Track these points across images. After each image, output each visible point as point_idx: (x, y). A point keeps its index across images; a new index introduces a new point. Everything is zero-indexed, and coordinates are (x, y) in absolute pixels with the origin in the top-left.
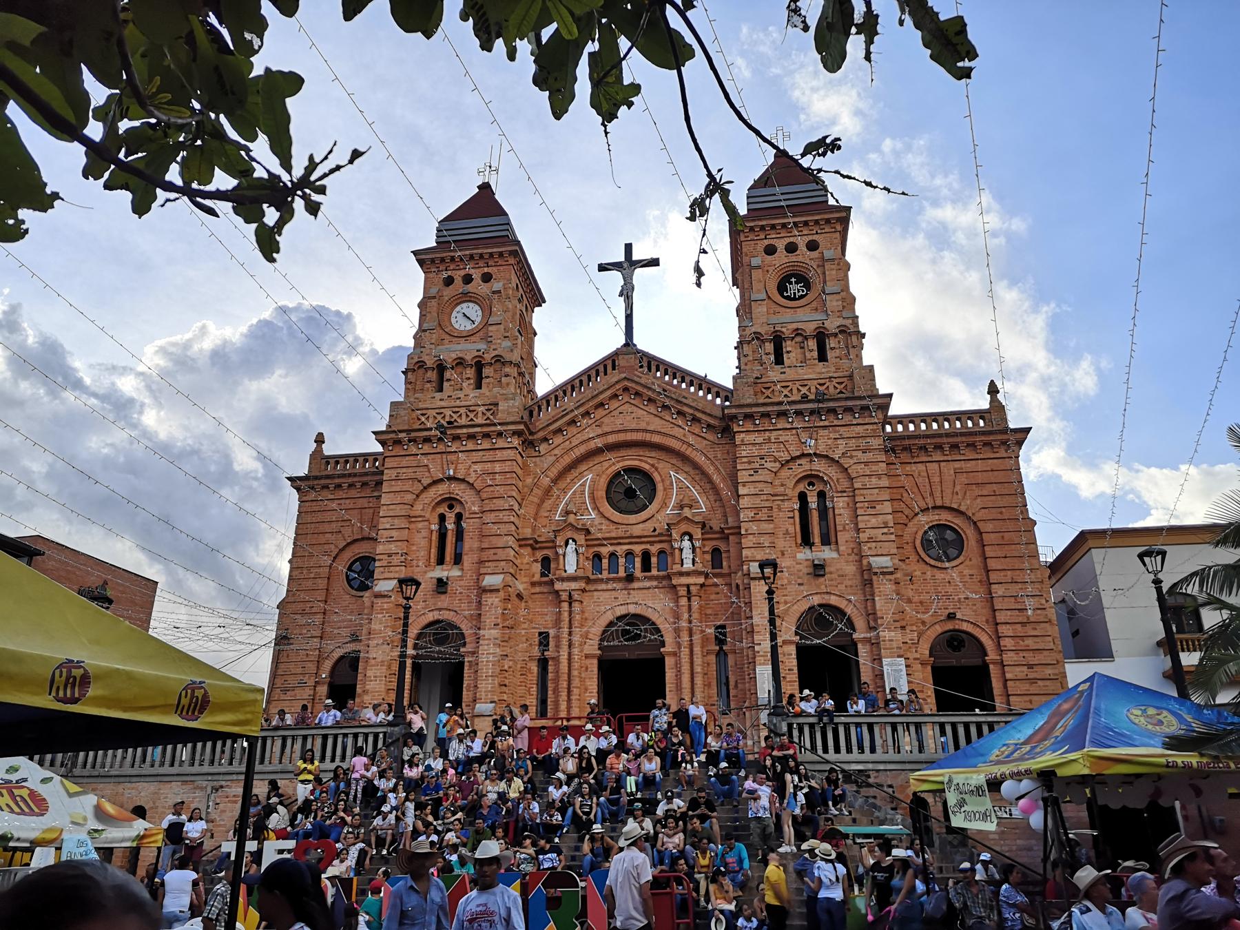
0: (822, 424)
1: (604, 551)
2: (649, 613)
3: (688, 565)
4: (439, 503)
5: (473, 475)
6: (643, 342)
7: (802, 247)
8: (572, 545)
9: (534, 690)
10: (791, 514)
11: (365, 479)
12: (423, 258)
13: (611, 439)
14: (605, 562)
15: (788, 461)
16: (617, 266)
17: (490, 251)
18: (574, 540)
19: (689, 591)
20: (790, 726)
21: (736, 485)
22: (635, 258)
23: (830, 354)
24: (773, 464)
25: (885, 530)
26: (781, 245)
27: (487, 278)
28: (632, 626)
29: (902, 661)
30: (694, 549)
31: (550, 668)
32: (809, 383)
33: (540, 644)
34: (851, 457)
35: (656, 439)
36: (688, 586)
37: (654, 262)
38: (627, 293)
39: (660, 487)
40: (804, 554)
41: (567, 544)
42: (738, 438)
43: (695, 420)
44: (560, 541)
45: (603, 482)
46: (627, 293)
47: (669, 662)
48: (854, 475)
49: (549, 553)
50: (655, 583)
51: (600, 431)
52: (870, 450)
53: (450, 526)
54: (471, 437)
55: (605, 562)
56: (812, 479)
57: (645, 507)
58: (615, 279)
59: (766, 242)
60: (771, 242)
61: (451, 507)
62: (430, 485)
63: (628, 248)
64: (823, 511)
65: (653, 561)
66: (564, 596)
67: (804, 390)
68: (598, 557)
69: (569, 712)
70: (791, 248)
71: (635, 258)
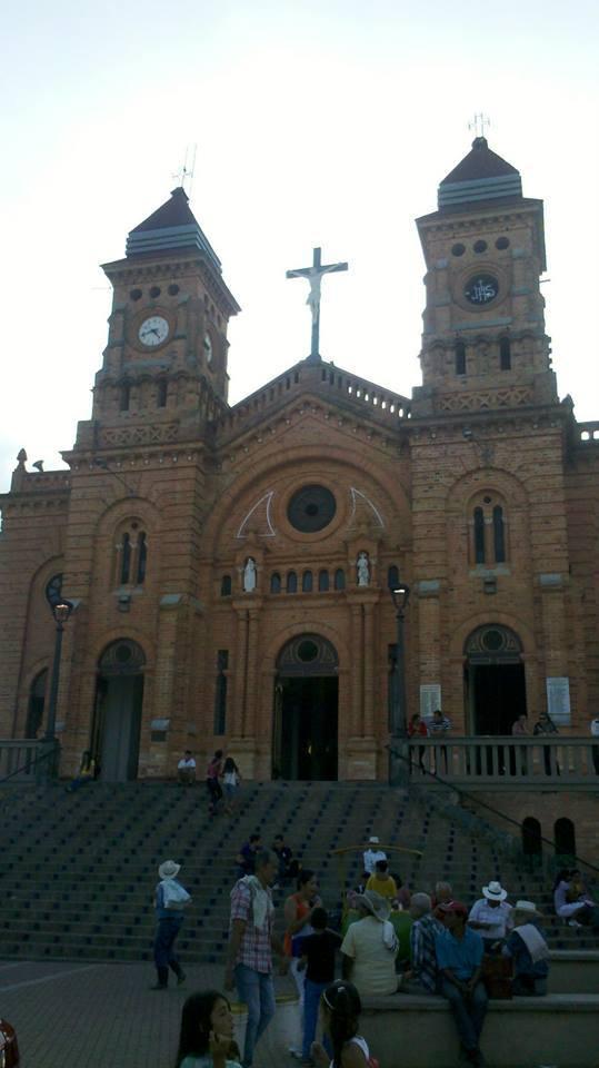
0: (499, 436)
1: (284, 569)
2: (324, 631)
3: (363, 583)
4: (123, 523)
5: (155, 494)
6: (326, 357)
7: (491, 245)
8: (250, 566)
9: (213, 706)
10: (465, 531)
11: (37, 499)
12: (112, 270)
13: (292, 455)
14: (284, 580)
15: (463, 476)
16: (304, 272)
17: (176, 261)
18: (253, 560)
19: (248, 615)
20: (411, 748)
21: (411, 500)
22: (323, 263)
23: (515, 361)
24: (447, 480)
25: (558, 547)
26: (469, 244)
27: (174, 290)
28: (308, 646)
29: (566, 681)
30: (369, 566)
31: (228, 685)
32: (490, 392)
33: (220, 661)
34: (528, 470)
35: (337, 454)
36: (362, 605)
37: (343, 267)
38: (314, 302)
39: (340, 504)
40: (481, 572)
41: (246, 562)
42: (415, 452)
43: (374, 433)
44: (239, 559)
45: (285, 498)
46: (314, 302)
47: (342, 681)
48: (530, 489)
49: (229, 572)
50: (332, 602)
51: (280, 447)
52: (548, 463)
53: (133, 545)
54: (152, 456)
55: (284, 580)
56: (488, 494)
57: (326, 523)
58: (303, 284)
59: (454, 242)
60: (460, 241)
61: (135, 526)
62: (114, 504)
63: (317, 252)
64: (499, 526)
65: (333, 581)
66: (242, 614)
67: (484, 401)
68: (277, 575)
69: (243, 730)
70: (480, 247)
71: (323, 263)
